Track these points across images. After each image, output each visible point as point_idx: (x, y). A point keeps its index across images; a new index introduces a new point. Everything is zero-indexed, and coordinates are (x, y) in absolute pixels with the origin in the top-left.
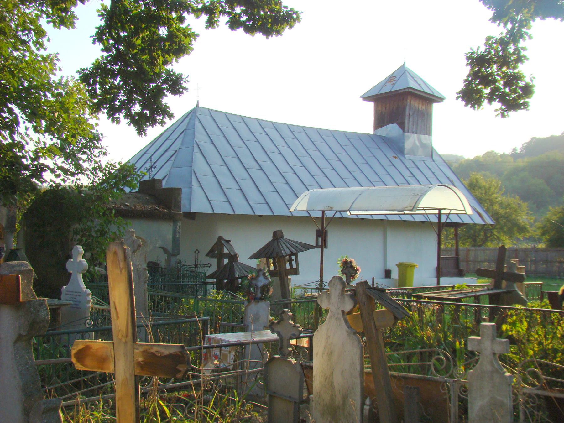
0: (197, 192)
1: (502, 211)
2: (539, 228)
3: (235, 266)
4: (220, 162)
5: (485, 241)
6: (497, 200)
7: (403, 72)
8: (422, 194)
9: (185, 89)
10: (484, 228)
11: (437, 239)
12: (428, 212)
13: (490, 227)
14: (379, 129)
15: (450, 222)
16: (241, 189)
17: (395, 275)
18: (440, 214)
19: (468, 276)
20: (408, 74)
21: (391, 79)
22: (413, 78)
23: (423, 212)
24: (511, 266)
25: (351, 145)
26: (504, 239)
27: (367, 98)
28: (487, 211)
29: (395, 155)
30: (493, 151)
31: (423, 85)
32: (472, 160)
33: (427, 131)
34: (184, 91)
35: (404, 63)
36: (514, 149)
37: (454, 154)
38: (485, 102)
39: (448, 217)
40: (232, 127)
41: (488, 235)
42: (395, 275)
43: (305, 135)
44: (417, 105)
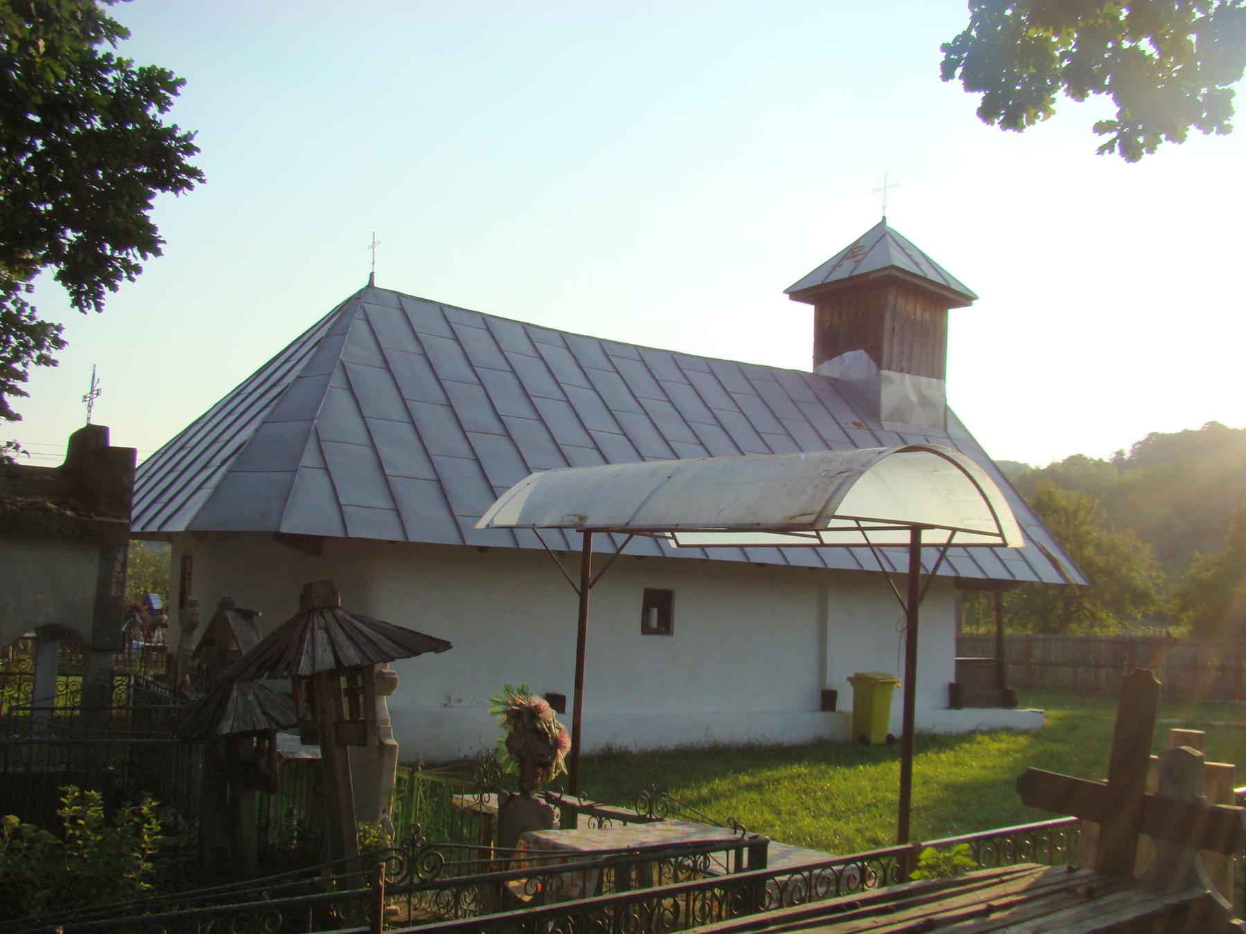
0: (312, 481)
1: (1099, 560)
2: (1174, 596)
3: (234, 694)
4: (397, 412)
5: (1067, 618)
6: (1091, 537)
7: (880, 235)
8: (845, 479)
9: (194, 173)
10: (1064, 590)
11: (903, 623)
12: (876, 537)
13: (1078, 593)
14: (826, 364)
15: (950, 573)
16: (439, 481)
17: (846, 703)
18: (915, 547)
19: (1026, 705)
20: (890, 240)
21: (853, 252)
22: (902, 249)
23: (856, 538)
24: (1180, 768)
25: (752, 392)
26: (1104, 616)
27: (798, 293)
28: (1072, 559)
29: (858, 421)
30: (1081, 456)
31: (924, 266)
32: (1043, 471)
33: (936, 369)
34: (194, 181)
35: (884, 218)
36: (1120, 454)
37: (1011, 460)
38: (1061, 98)
39: (943, 555)
40: (449, 334)
41: (1073, 609)
42: (846, 703)
43: (640, 367)
44: (910, 308)
